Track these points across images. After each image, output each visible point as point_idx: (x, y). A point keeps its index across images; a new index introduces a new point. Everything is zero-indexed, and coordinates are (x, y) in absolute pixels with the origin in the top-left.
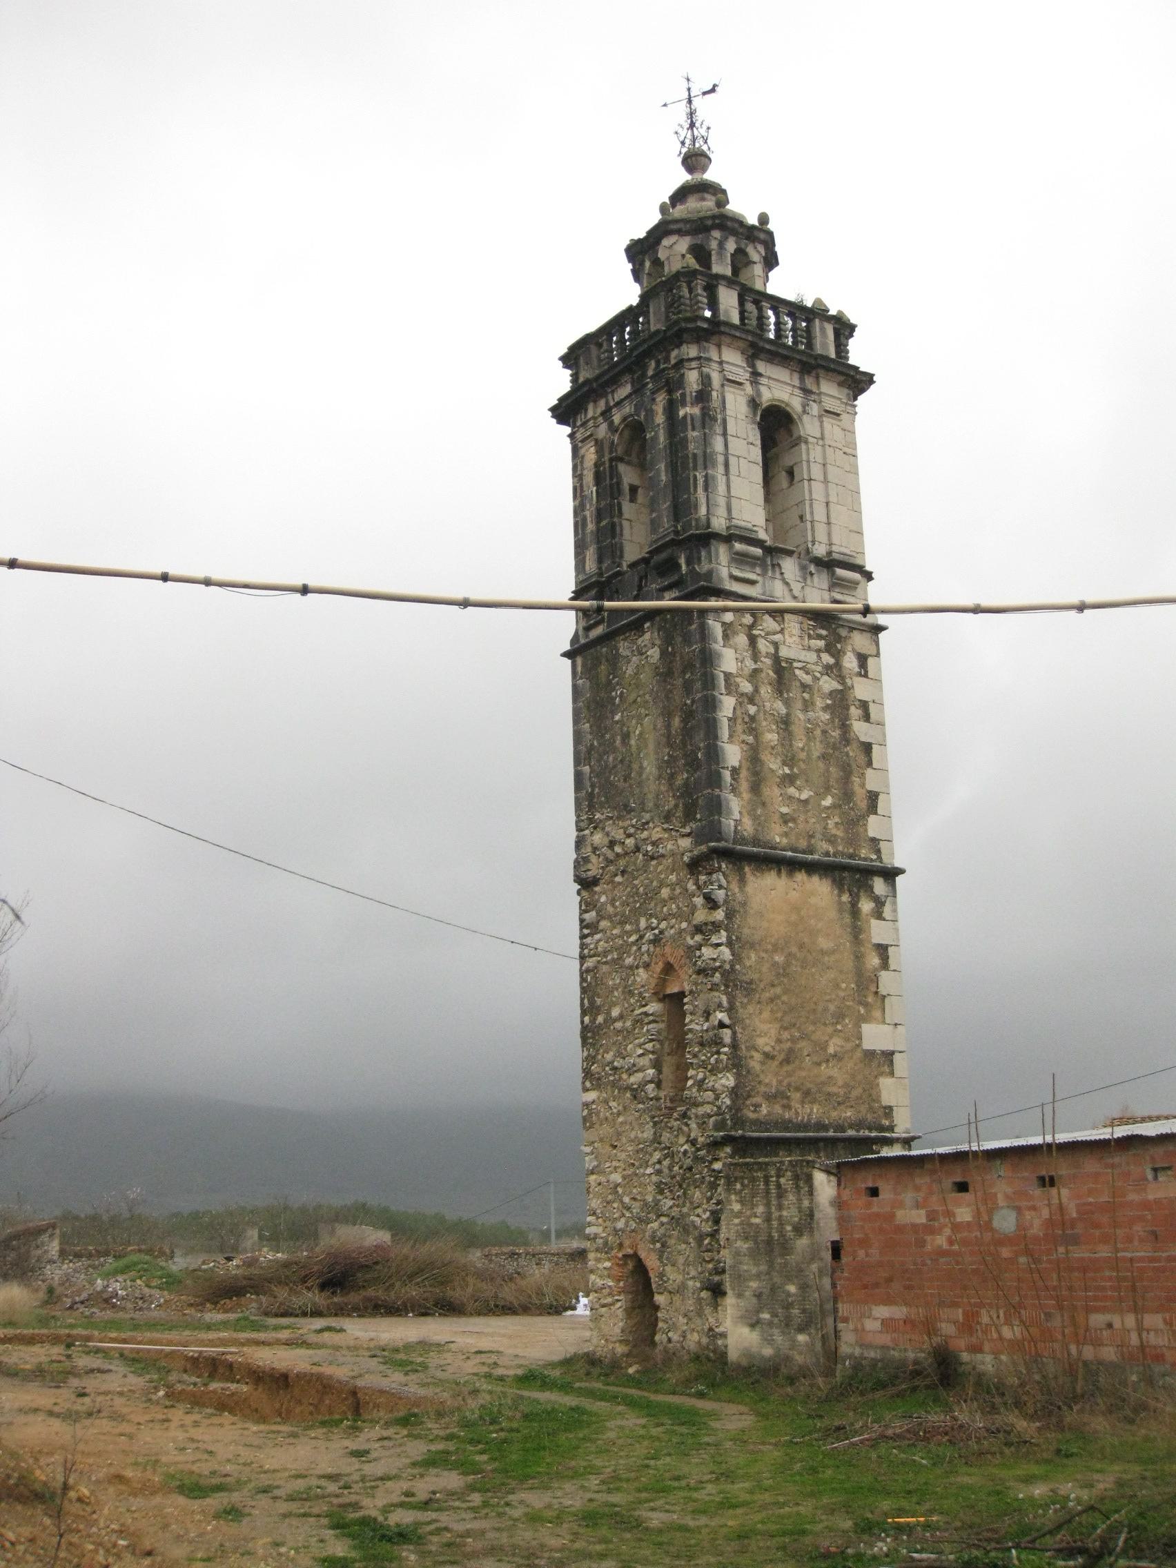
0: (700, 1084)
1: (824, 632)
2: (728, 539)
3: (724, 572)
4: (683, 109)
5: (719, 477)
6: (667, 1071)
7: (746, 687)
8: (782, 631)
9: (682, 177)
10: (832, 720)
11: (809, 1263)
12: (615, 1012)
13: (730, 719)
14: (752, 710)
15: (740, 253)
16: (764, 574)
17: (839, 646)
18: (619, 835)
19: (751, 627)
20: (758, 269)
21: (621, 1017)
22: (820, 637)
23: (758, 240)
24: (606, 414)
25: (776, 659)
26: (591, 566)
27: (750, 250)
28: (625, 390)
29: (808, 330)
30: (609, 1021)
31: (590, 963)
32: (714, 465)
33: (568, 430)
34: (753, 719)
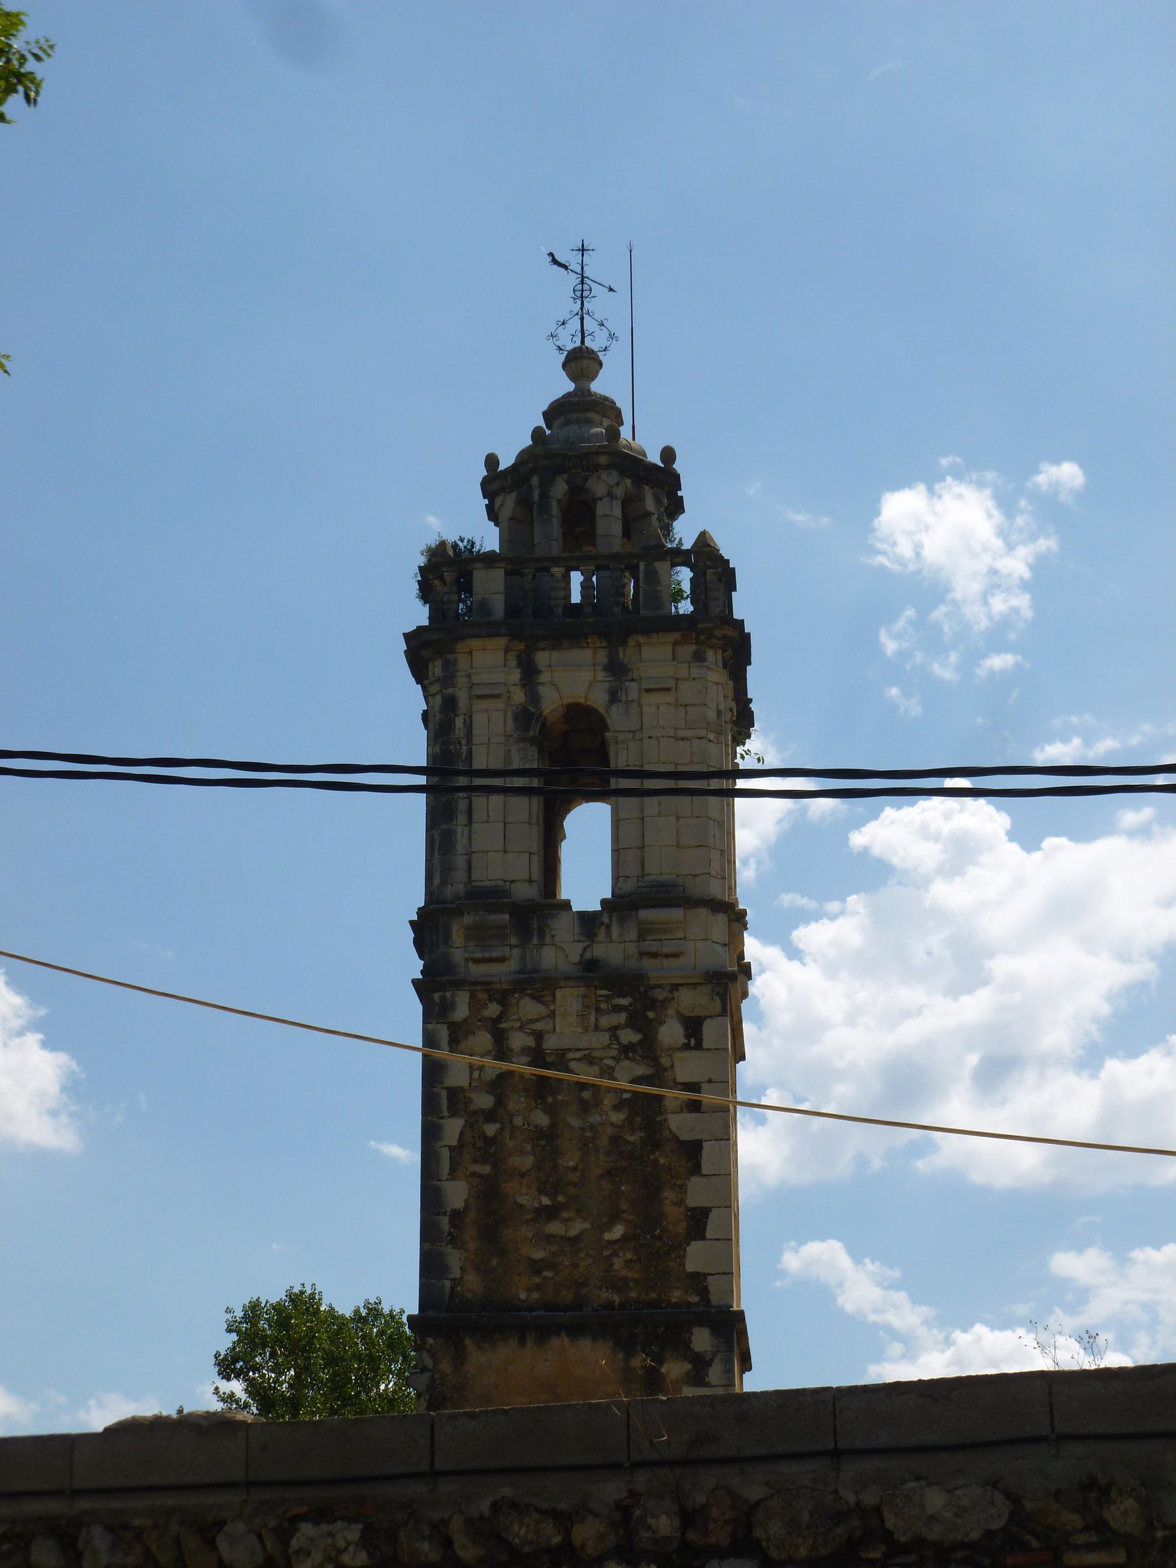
1: (624, 1002)
5: (459, 829)
7: (484, 1101)
8: (552, 1015)
10: (630, 1121)
13: (451, 1148)
14: (491, 1129)
17: (651, 1015)
22: (618, 1009)
34: (491, 1141)
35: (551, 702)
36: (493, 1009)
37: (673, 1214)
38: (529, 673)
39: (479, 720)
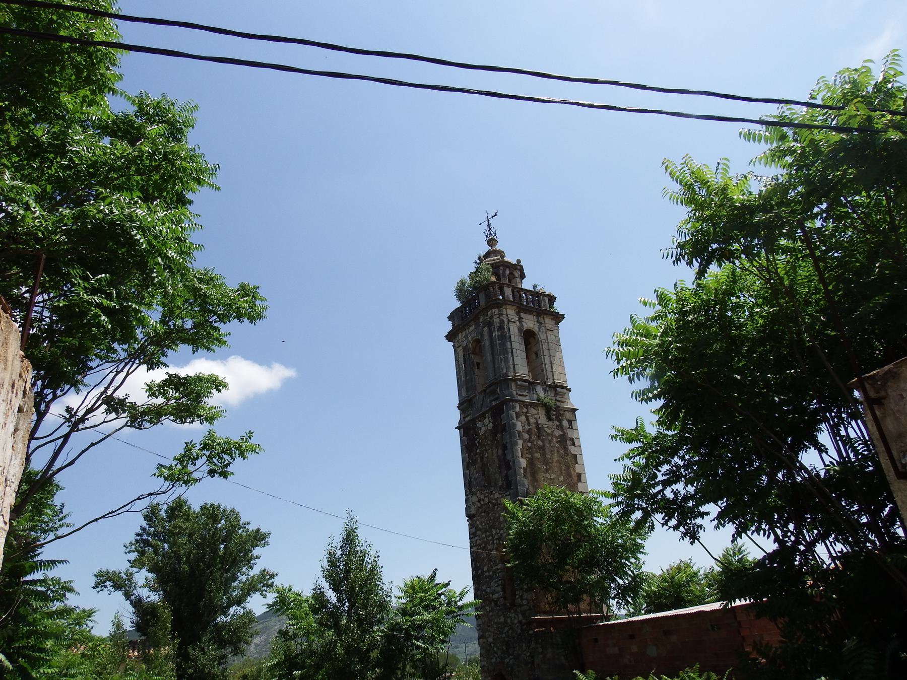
0: (521, 597)
2: (515, 380)
3: (515, 393)
12: (485, 569)
15: (511, 273)
18: (482, 497)
20: (518, 280)
21: (488, 571)
24: (466, 337)
25: (537, 424)
26: (464, 394)
28: (472, 328)
30: (483, 572)
31: (475, 549)
32: (507, 353)
35: (525, 327)
36: (525, 410)
37: (574, 474)
38: (520, 319)
39: (511, 328)
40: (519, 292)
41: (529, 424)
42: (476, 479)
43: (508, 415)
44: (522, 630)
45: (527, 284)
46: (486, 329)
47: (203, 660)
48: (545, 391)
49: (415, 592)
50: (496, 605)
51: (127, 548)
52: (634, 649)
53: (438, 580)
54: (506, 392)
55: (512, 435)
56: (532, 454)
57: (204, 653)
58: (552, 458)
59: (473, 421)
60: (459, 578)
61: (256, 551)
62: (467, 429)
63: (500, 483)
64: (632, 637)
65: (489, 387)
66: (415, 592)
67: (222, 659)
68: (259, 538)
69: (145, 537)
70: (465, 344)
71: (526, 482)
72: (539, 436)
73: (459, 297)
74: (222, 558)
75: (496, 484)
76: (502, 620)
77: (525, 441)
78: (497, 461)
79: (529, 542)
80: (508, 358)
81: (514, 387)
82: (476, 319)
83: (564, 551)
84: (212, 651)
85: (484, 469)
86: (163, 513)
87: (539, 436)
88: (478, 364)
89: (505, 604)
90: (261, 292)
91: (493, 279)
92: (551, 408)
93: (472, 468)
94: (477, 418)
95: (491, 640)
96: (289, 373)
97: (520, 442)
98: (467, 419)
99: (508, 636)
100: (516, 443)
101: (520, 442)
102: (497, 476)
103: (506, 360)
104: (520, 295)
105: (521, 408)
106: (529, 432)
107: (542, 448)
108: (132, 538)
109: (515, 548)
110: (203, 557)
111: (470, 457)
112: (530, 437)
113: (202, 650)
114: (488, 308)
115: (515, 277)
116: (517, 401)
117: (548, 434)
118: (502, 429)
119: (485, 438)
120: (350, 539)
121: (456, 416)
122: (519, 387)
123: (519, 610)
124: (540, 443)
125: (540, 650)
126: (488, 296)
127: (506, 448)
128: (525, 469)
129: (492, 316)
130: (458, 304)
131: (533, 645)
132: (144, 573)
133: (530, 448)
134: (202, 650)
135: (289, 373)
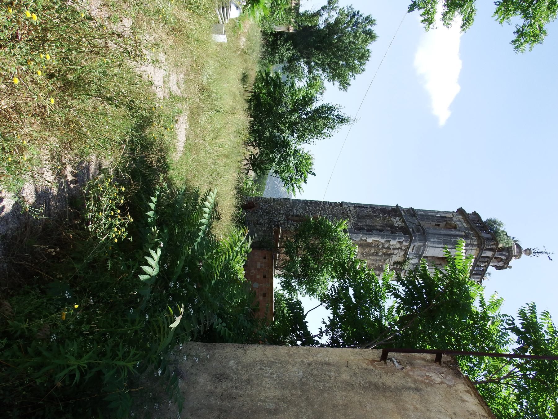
0: (292, 224)
2: (424, 246)
3: (416, 244)
4: (544, 251)
6: (296, 218)
9: (524, 248)
11: (239, 19)
12: (310, 208)
15: (502, 260)
16: (414, 253)
18: (352, 213)
19: (401, 249)
20: (496, 264)
21: (309, 209)
23: (504, 264)
24: (459, 221)
25: (393, 254)
26: (419, 213)
27: (502, 262)
28: (465, 225)
29: (478, 274)
30: (309, 206)
31: (322, 203)
32: (444, 244)
33: (455, 211)
36: (403, 248)
40: (487, 261)
41: (393, 249)
42: (364, 211)
43: (402, 236)
44: (275, 221)
45: (491, 269)
46: (463, 234)
47: (283, 50)
48: (413, 264)
49: (306, 159)
50: (290, 210)
51: (350, 7)
52: (258, 277)
53: (309, 175)
54: (417, 238)
55: (388, 236)
56: (374, 247)
57: (287, 50)
58: (369, 259)
59: (401, 215)
60: (309, 191)
61: (337, 84)
62: (396, 211)
63: (359, 224)
64: (264, 277)
65: (422, 228)
66: (306, 159)
67: (281, 60)
68: (345, 84)
69: (356, 17)
70: (454, 219)
71: (358, 240)
72: (385, 254)
73: (489, 221)
74: (338, 63)
75: (359, 222)
76: (282, 212)
77: (383, 244)
78: (374, 224)
79: (323, 232)
80: (441, 244)
81: (419, 244)
82: (472, 229)
83: (315, 253)
84: (287, 55)
85: (369, 216)
86: (369, 27)
87: (385, 254)
88: (439, 225)
89: (290, 215)
90: (536, 46)
91: (500, 246)
92: (402, 266)
93: (370, 209)
94: (402, 218)
95: (272, 204)
96: (442, 122)
97: (383, 241)
98: (402, 212)
99: (273, 213)
100: (383, 238)
101: (383, 241)
102: (364, 223)
103: (439, 243)
104: (485, 262)
105: (405, 246)
106: (388, 248)
107: (377, 254)
108: (356, 9)
109: (321, 223)
110: (340, 50)
111: (378, 209)
112: (385, 248)
113: (289, 50)
114: (479, 238)
115: (498, 262)
116: (410, 244)
117: (385, 260)
118: (393, 231)
119: (388, 221)
120: (342, 120)
121: (405, 205)
122: (419, 248)
123: (286, 222)
124: (380, 254)
125: (263, 229)
126: (488, 239)
127: (380, 232)
128: (365, 240)
129: (472, 239)
130: (484, 219)
131: (266, 226)
132: (336, 16)
133: (378, 247)
134: (289, 50)
135: (442, 122)
